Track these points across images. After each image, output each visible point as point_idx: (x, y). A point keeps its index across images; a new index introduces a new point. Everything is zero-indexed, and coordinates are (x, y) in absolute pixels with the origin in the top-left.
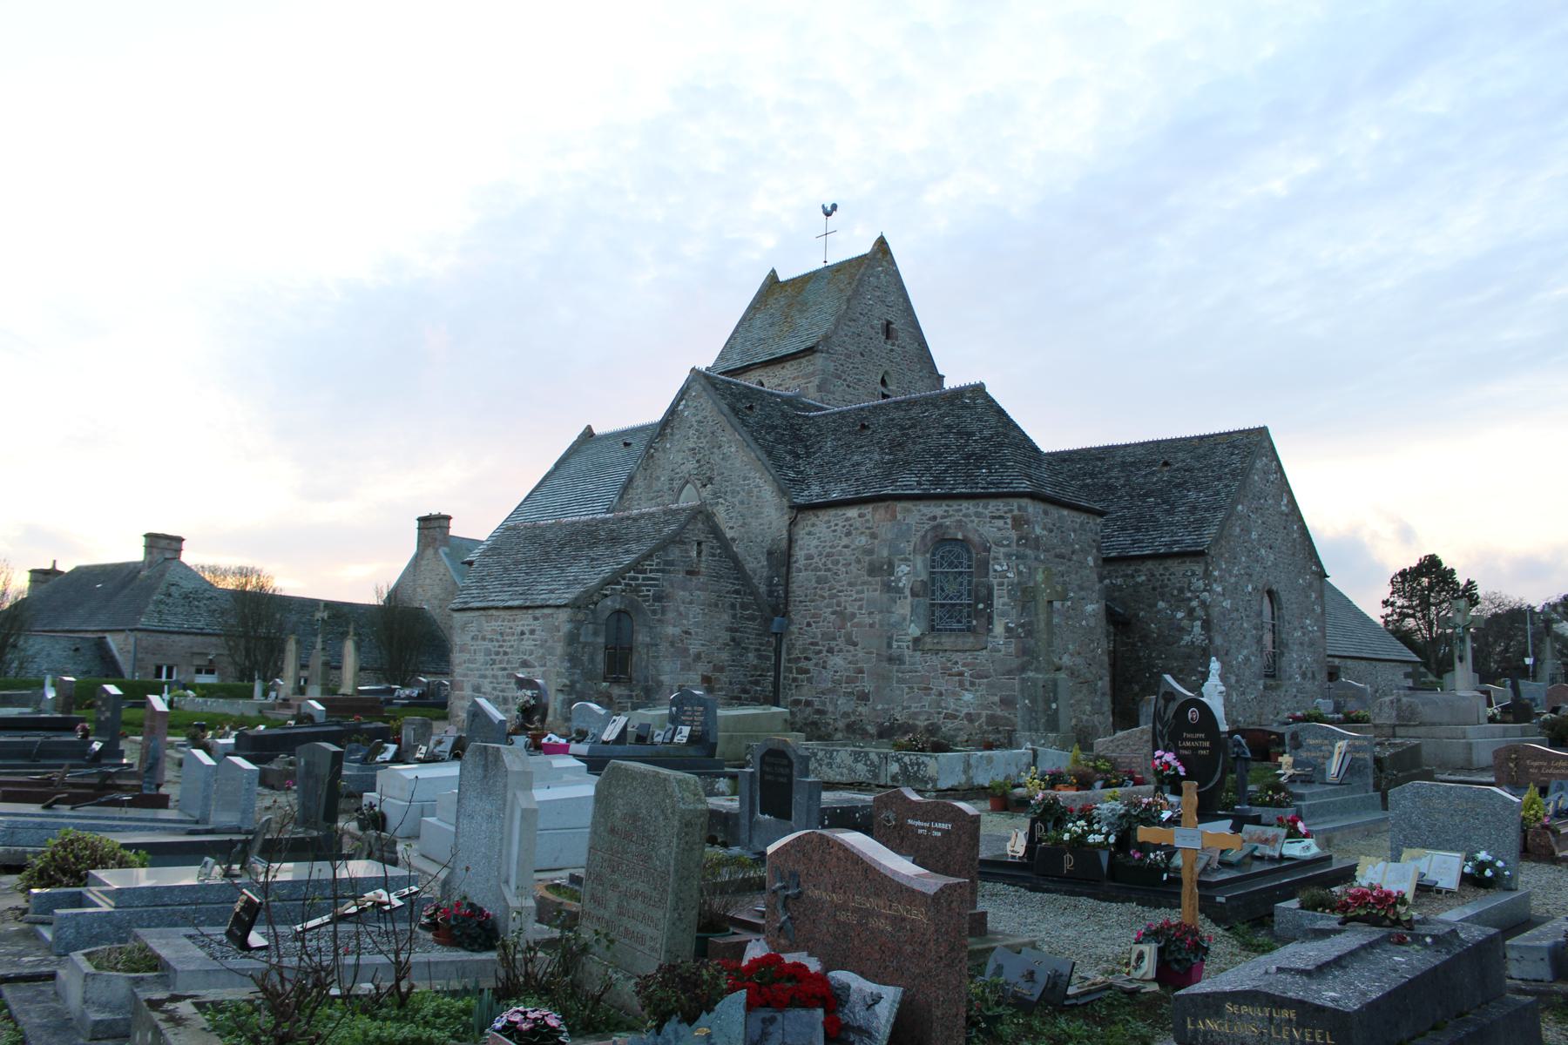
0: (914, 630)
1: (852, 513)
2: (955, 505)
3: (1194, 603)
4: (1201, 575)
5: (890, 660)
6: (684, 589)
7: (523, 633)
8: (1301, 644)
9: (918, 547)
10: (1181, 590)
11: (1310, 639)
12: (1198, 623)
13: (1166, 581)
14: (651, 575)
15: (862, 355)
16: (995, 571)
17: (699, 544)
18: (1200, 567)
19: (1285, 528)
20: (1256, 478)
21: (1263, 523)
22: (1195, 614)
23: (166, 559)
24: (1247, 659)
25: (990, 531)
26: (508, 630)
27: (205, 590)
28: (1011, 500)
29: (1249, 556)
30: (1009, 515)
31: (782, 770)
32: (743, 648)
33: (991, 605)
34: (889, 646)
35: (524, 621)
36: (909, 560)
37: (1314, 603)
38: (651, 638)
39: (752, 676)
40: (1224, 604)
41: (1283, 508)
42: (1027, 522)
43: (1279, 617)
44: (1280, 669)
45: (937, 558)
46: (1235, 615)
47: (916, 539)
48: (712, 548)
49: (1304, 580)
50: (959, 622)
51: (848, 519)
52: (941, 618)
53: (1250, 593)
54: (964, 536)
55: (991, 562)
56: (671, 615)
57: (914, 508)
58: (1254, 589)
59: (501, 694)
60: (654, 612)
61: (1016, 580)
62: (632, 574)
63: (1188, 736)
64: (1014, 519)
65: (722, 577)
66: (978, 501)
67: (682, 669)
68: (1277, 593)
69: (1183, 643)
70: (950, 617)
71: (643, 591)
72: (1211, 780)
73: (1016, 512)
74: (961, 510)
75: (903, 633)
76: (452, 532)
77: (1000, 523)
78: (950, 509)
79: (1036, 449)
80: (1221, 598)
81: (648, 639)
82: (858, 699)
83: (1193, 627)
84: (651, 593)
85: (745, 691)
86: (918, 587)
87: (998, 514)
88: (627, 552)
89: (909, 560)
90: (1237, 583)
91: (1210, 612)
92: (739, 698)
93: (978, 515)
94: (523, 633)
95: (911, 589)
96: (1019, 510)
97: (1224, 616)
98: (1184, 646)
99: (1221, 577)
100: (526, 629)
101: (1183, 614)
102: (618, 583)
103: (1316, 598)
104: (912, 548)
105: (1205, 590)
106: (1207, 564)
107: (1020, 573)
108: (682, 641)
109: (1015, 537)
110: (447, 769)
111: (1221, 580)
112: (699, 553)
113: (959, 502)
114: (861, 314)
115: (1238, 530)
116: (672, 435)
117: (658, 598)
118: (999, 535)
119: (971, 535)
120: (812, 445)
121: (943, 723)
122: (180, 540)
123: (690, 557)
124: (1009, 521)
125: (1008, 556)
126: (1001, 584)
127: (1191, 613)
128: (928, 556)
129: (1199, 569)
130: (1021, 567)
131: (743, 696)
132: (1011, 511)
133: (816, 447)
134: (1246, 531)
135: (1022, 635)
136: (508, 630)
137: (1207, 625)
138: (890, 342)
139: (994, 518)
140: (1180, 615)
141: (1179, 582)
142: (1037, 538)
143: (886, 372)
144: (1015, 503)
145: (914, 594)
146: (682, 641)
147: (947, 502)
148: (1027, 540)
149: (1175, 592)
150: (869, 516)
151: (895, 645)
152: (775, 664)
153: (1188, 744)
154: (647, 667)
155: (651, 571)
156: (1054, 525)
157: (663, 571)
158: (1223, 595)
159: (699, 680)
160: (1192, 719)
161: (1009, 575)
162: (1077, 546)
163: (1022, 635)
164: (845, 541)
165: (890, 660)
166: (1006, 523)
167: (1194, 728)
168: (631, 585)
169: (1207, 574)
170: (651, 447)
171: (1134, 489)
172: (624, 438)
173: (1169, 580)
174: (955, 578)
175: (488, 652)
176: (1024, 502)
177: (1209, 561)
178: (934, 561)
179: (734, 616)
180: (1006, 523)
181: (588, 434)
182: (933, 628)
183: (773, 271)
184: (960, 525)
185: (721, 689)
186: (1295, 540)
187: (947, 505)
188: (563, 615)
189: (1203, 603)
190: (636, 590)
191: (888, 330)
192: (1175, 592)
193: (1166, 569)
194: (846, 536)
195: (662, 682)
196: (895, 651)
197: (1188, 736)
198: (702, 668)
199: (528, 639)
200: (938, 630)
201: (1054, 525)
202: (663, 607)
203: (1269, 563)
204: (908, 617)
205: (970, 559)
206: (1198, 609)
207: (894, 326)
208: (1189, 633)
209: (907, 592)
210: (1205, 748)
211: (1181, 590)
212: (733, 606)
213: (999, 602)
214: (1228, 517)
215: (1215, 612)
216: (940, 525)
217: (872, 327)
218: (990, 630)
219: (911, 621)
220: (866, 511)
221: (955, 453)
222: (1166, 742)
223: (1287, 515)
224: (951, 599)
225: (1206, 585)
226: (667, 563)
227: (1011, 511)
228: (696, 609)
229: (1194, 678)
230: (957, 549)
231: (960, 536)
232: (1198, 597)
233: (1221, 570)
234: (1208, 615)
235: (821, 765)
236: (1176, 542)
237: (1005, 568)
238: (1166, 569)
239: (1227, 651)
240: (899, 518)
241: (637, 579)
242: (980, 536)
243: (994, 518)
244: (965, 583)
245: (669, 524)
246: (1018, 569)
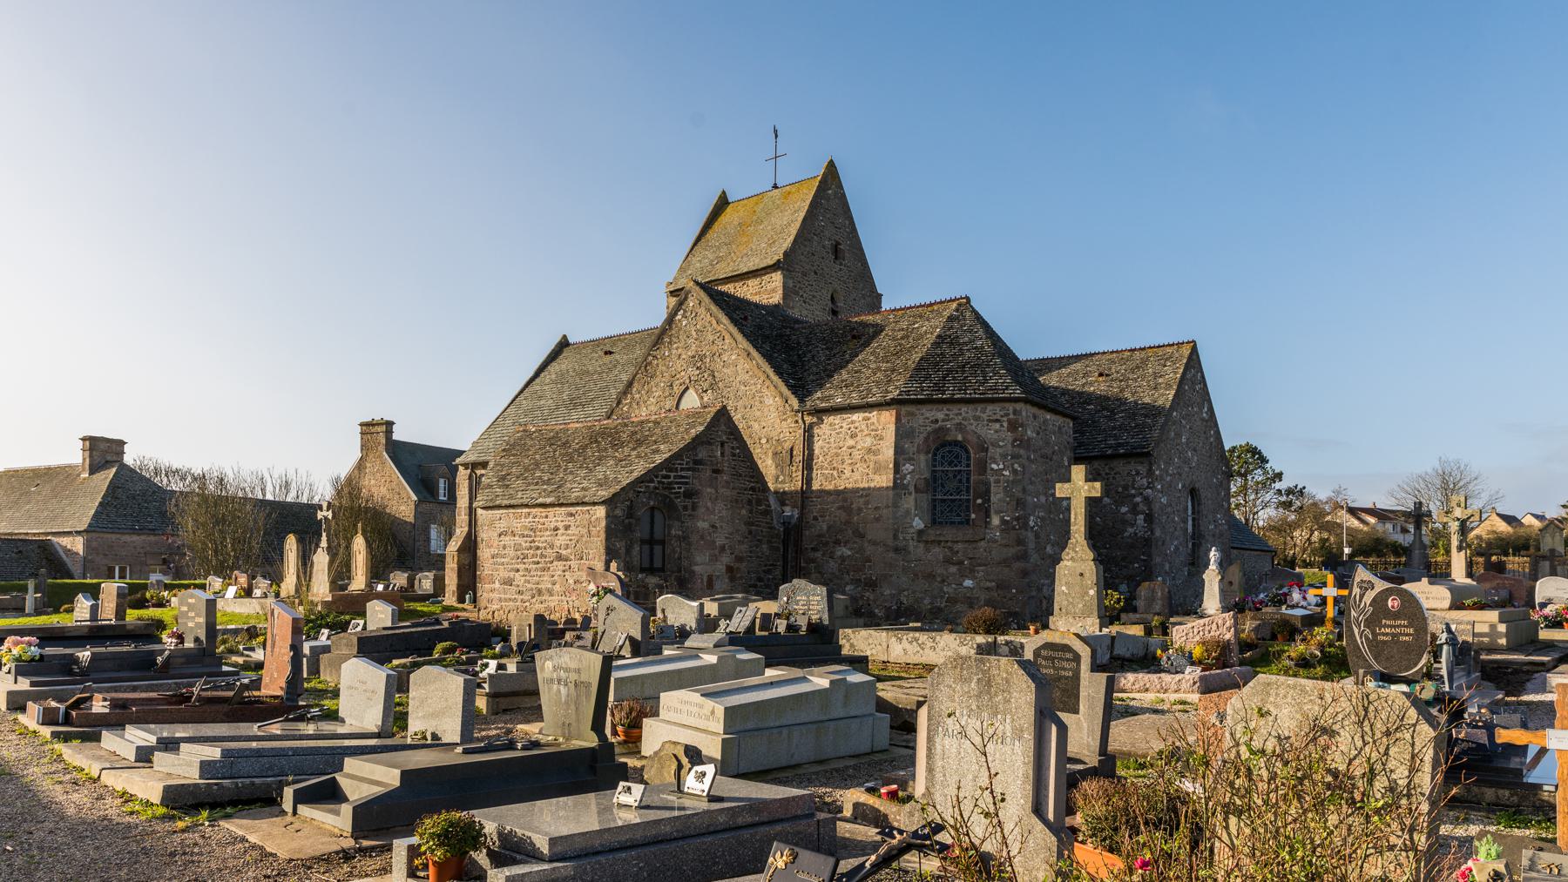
0: (918, 523)
1: (857, 417)
2: (955, 409)
3: (1138, 499)
4: (1145, 474)
5: (897, 550)
6: (711, 486)
7: (556, 529)
8: (1214, 536)
9: (921, 447)
10: (1126, 488)
11: (1220, 531)
12: (1142, 517)
13: (1111, 480)
14: (683, 473)
15: (816, 273)
16: (992, 469)
17: (722, 444)
18: (1144, 467)
19: (1205, 433)
20: (1187, 387)
21: (1190, 428)
22: (1139, 509)
23: (107, 462)
24: (1177, 548)
25: (990, 432)
26: (540, 526)
27: (154, 492)
28: (1007, 405)
29: (1180, 458)
30: (1005, 419)
31: (1066, 665)
32: (758, 540)
33: (989, 500)
34: (895, 537)
35: (557, 516)
36: (913, 459)
37: (1223, 500)
38: (683, 532)
39: (766, 566)
40: (1162, 500)
41: (1205, 415)
42: (1022, 425)
43: (1198, 512)
44: (1198, 557)
45: (938, 457)
46: (1169, 509)
47: (920, 440)
48: (733, 448)
49: (1217, 479)
50: (958, 515)
51: (853, 422)
52: (942, 513)
53: (1180, 490)
54: (964, 438)
55: (989, 461)
56: (702, 510)
57: (918, 412)
58: (1183, 487)
59: (534, 586)
60: (685, 508)
61: (1011, 479)
62: (664, 472)
63: (1388, 622)
64: (1009, 421)
65: (740, 475)
66: (977, 405)
67: (710, 560)
68: (1198, 490)
69: (1126, 534)
70: (951, 511)
71: (674, 488)
72: (1416, 665)
73: (1011, 416)
74: (961, 414)
75: (908, 525)
76: (394, 438)
77: (997, 426)
78: (951, 413)
79: (1016, 359)
80: (1160, 495)
81: (680, 533)
82: (866, 585)
83: (1136, 520)
84: (682, 490)
85: (760, 579)
86: (922, 485)
87: (995, 417)
88: (657, 451)
89: (913, 459)
90: (1171, 481)
91: (1153, 506)
92: (755, 586)
93: (977, 418)
94: (556, 529)
95: (915, 485)
96: (1014, 414)
97: (1162, 511)
98: (1128, 538)
99: (1161, 476)
100: (560, 525)
101: (1127, 509)
102: (652, 481)
103: (1225, 495)
104: (915, 449)
105: (1148, 487)
106: (1151, 464)
107: (1015, 472)
108: (710, 534)
109: (1011, 440)
110: (668, 665)
111: (1161, 478)
112: (722, 454)
113: (959, 406)
114: (814, 234)
115: (1173, 434)
116: (670, 343)
117: (689, 494)
118: (995, 436)
119: (969, 437)
120: (804, 354)
121: (946, 606)
122: (122, 443)
123: (715, 457)
124: (1005, 424)
125: (1004, 456)
126: (997, 482)
127: (1134, 510)
128: (930, 455)
129: (1143, 469)
130: (1016, 466)
131: (759, 584)
132: (1007, 415)
133: (809, 355)
134: (1179, 435)
135: (1017, 527)
136: (540, 526)
137: (1149, 518)
138: (838, 262)
139: (990, 421)
140: (1124, 509)
141: (1124, 480)
142: (1029, 439)
143: (835, 291)
144: (1010, 407)
145: (917, 490)
146: (710, 534)
147: (948, 406)
148: (1021, 441)
149: (1120, 489)
150: (874, 420)
151: (901, 537)
152: (783, 555)
153: (1388, 630)
154: (680, 558)
155: (682, 469)
156: (1040, 428)
157: (693, 470)
158: (1162, 492)
159: (724, 571)
160: (1393, 607)
161: (1004, 472)
162: (1056, 448)
163: (1017, 527)
164: (851, 442)
165: (897, 550)
166: (1002, 426)
167: (1396, 615)
168: (663, 483)
169: (1150, 472)
170: (649, 354)
171: (1073, 398)
172: (606, 347)
173: (1114, 478)
174: (955, 476)
175: (517, 548)
176: (1019, 406)
177: (1153, 462)
178: (935, 460)
179: (751, 512)
180: (1002, 426)
181: (564, 344)
182: (934, 522)
183: (724, 192)
184: (960, 427)
185: (741, 578)
186: (1211, 443)
187: (948, 410)
188: (601, 512)
189: (1146, 499)
190: (669, 487)
191: (836, 251)
192: (1120, 489)
193: (1111, 469)
194: (852, 437)
195: (694, 572)
196: (901, 544)
197: (1388, 622)
198: (726, 559)
199: (563, 534)
200: (940, 523)
201: (1040, 428)
202: (693, 503)
203: (1194, 464)
204: (913, 511)
205: (968, 458)
206: (1140, 505)
207: (841, 247)
208: (1132, 525)
209: (912, 489)
210: (1407, 635)
211: (1126, 488)
212: (750, 502)
213: (997, 496)
214: (1165, 424)
215: (1156, 507)
216: (941, 429)
217: (824, 247)
218: (989, 523)
219: (916, 515)
220: (871, 415)
221: (950, 362)
222: (1362, 628)
223: (1207, 421)
224: (951, 495)
225: (1149, 483)
226: (697, 462)
227: (1007, 415)
228: (720, 505)
229: (1136, 565)
230: (957, 449)
231: (960, 438)
232: (1141, 494)
233: (1161, 470)
234: (1150, 509)
235: (923, 649)
236: (1120, 445)
237: (1001, 466)
238: (1111, 469)
239: (1164, 541)
240: (903, 421)
241: (669, 477)
242: (979, 437)
243: (990, 421)
244: (964, 480)
245: (694, 427)
246: (1013, 468)
